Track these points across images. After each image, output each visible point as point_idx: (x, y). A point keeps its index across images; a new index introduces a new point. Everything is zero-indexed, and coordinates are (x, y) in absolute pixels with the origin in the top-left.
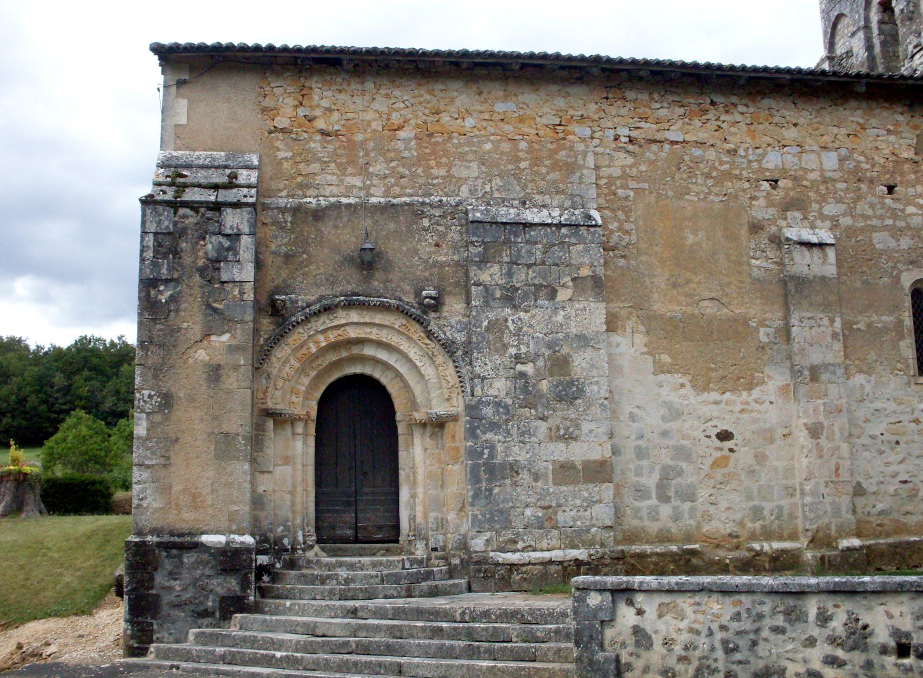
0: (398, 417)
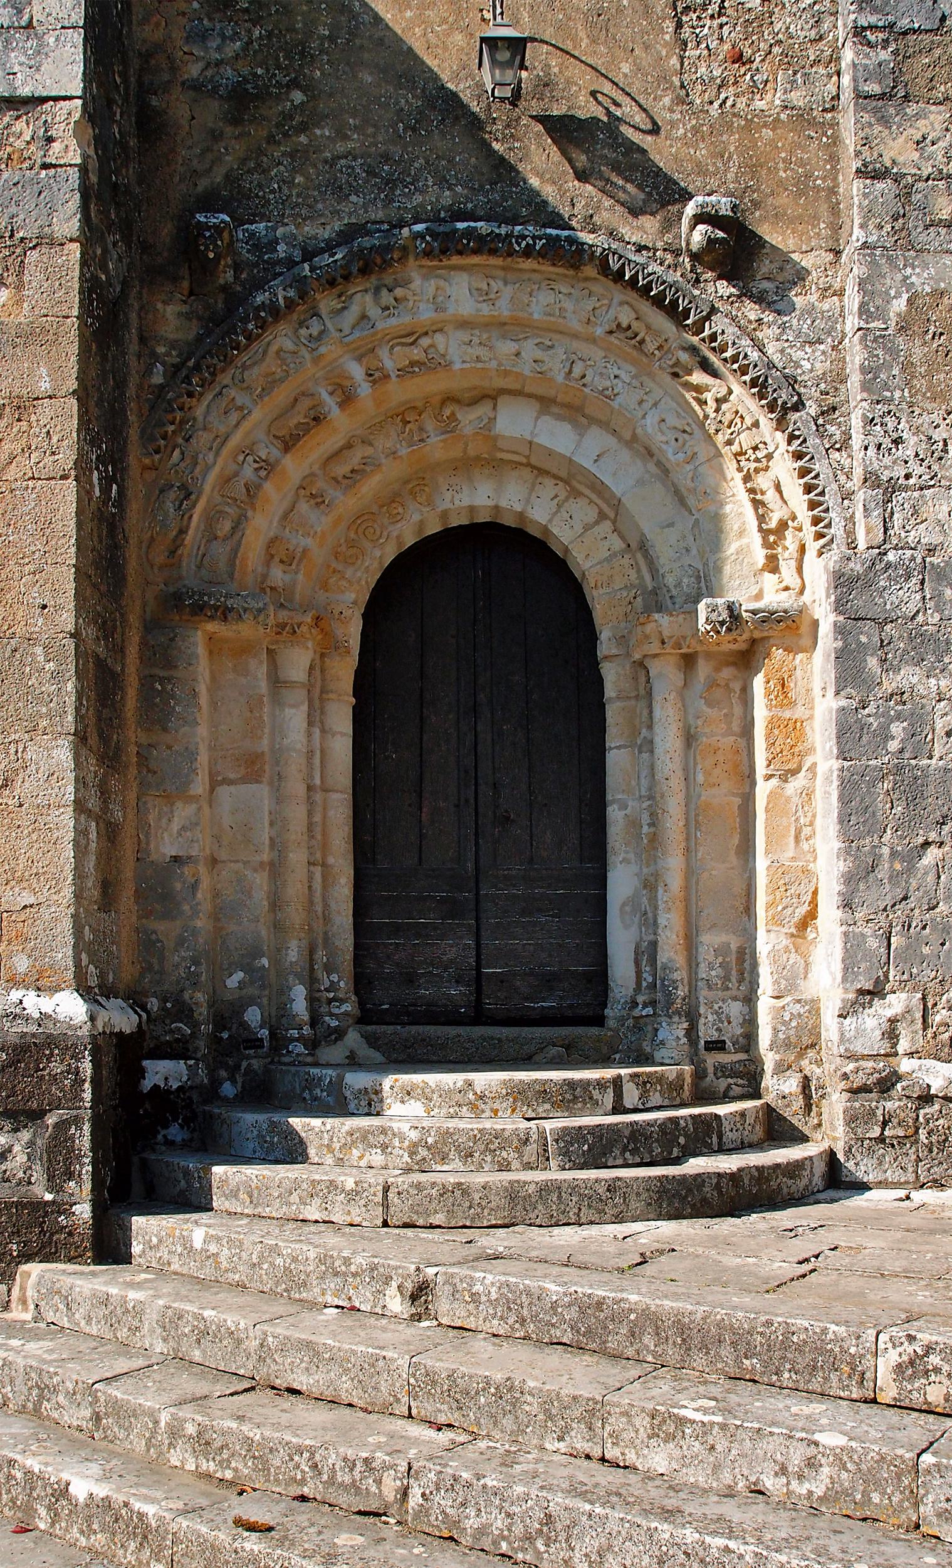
0: (605, 646)
